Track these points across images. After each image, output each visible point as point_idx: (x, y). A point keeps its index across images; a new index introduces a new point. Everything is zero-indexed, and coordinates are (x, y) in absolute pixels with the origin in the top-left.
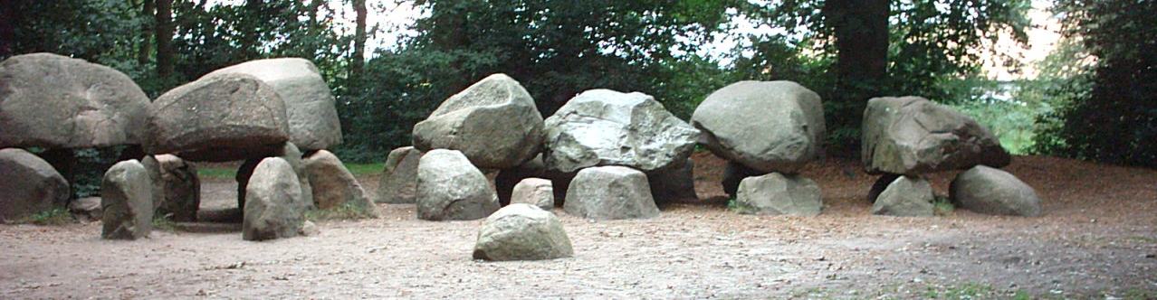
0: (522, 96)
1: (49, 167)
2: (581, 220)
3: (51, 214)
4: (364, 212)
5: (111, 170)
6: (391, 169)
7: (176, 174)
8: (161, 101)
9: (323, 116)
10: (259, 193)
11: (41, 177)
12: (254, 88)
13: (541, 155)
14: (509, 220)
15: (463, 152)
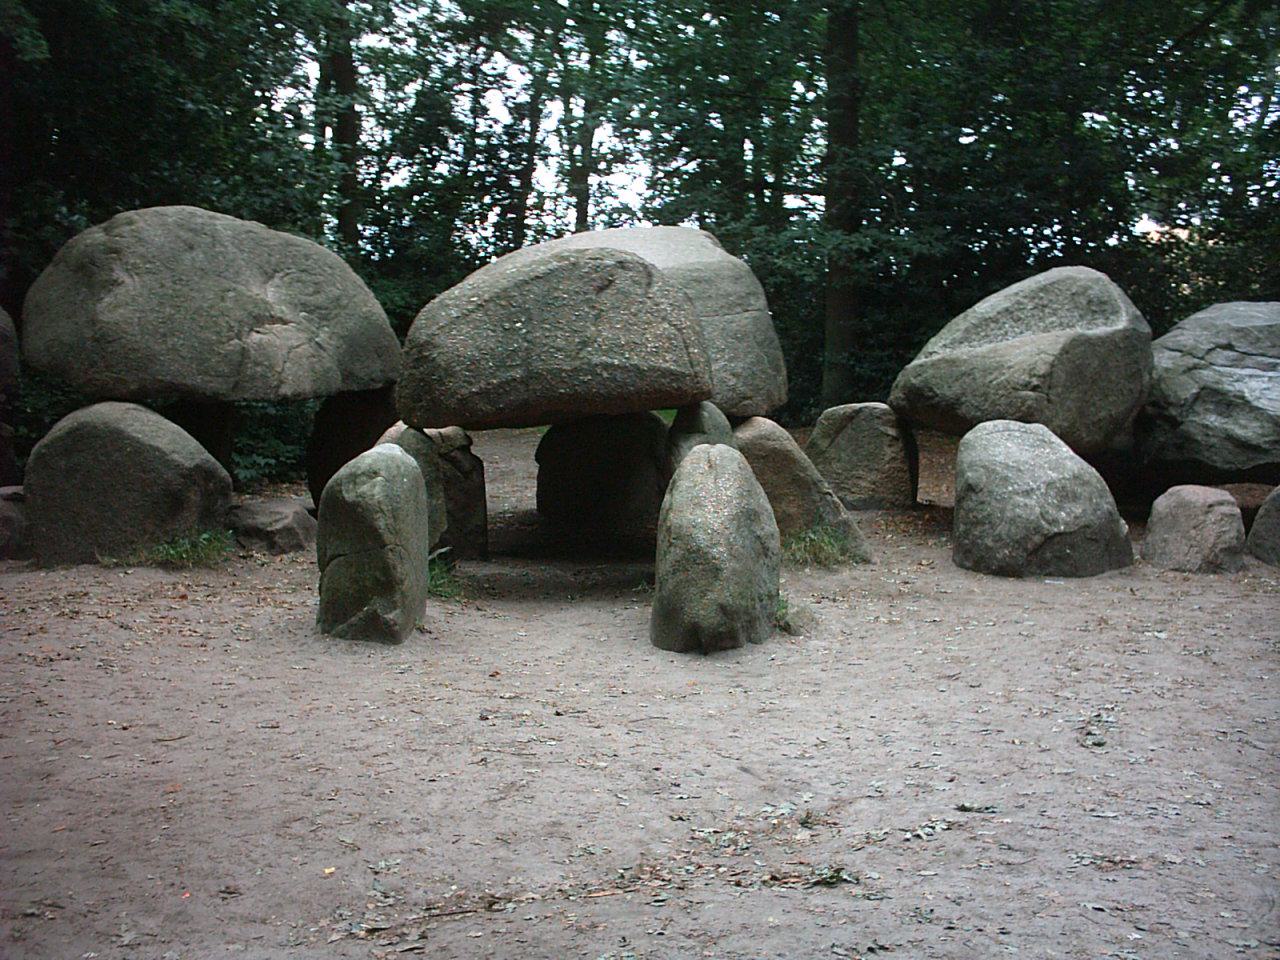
1: (193, 443)
3: (194, 545)
5: (343, 471)
6: (824, 444)
7: (453, 461)
9: (760, 344)
10: (702, 538)
12: (644, 281)
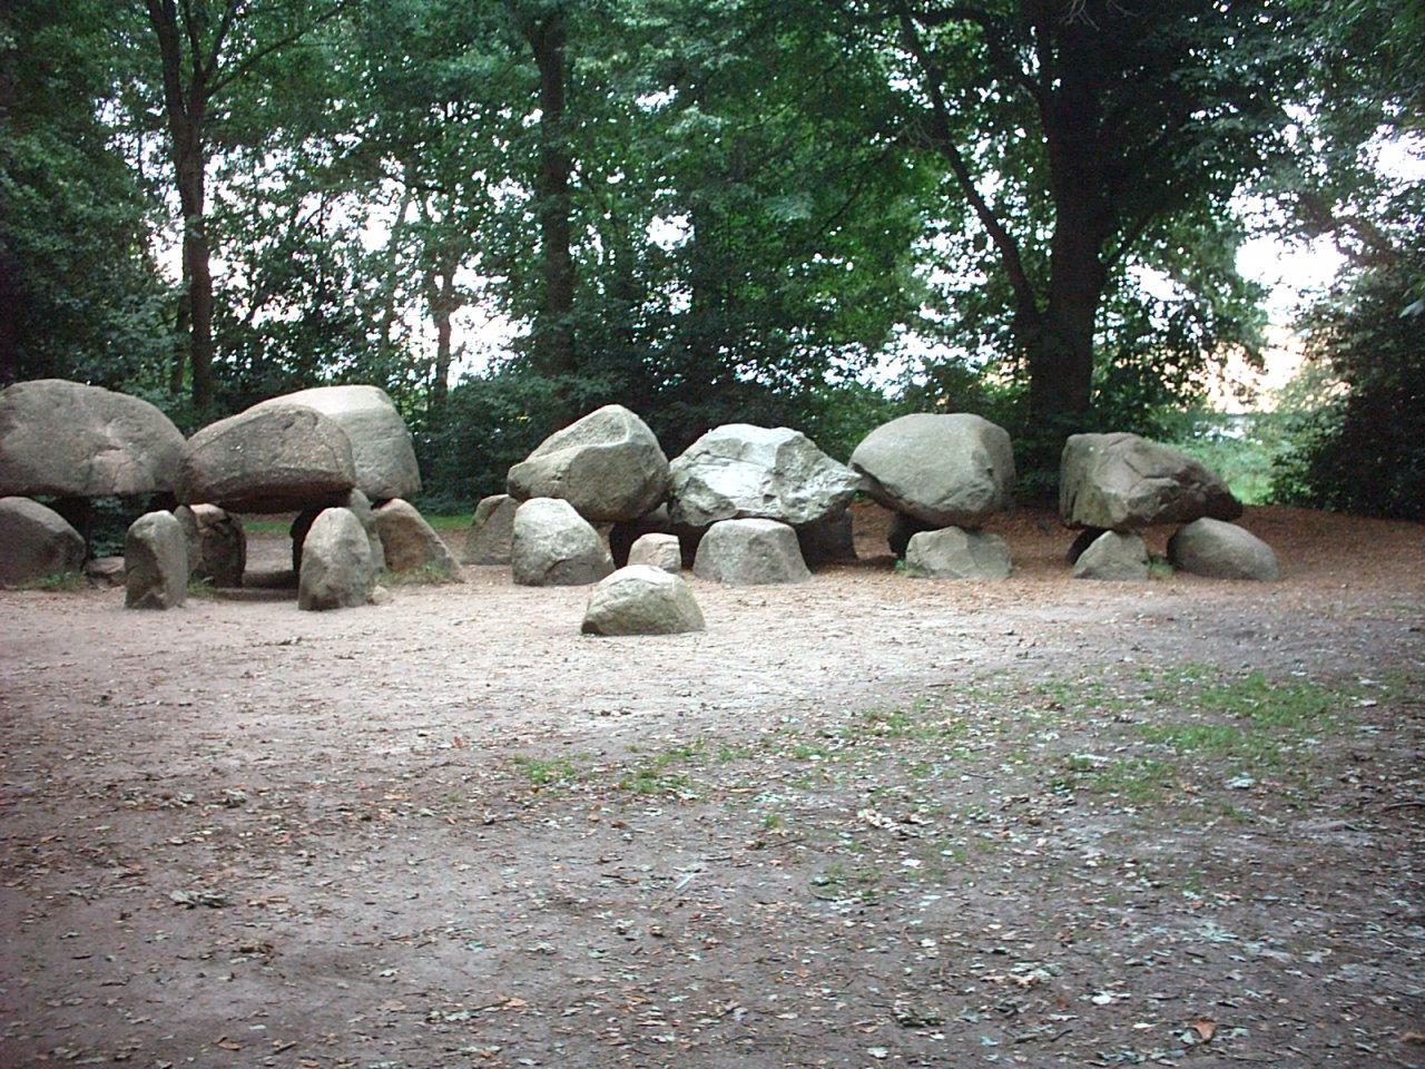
1: (60, 520)
4: (447, 576)
5: (136, 523)
6: (481, 522)
9: (397, 456)
10: (319, 552)
11: (51, 532)
13: (665, 504)
15: (569, 501)
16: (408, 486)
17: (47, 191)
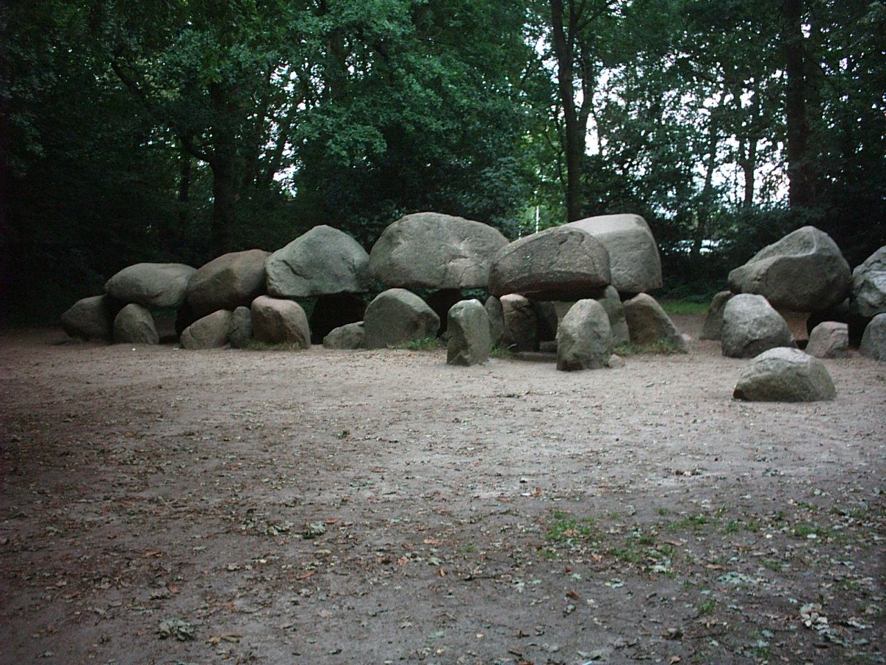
0: (827, 247)
2: (873, 362)
3: (422, 342)
4: (675, 348)
8: (504, 250)
10: (570, 330)
11: (416, 312)
13: (848, 300)
14: (769, 363)
15: (766, 297)
16: (651, 284)
17: (441, 91)
